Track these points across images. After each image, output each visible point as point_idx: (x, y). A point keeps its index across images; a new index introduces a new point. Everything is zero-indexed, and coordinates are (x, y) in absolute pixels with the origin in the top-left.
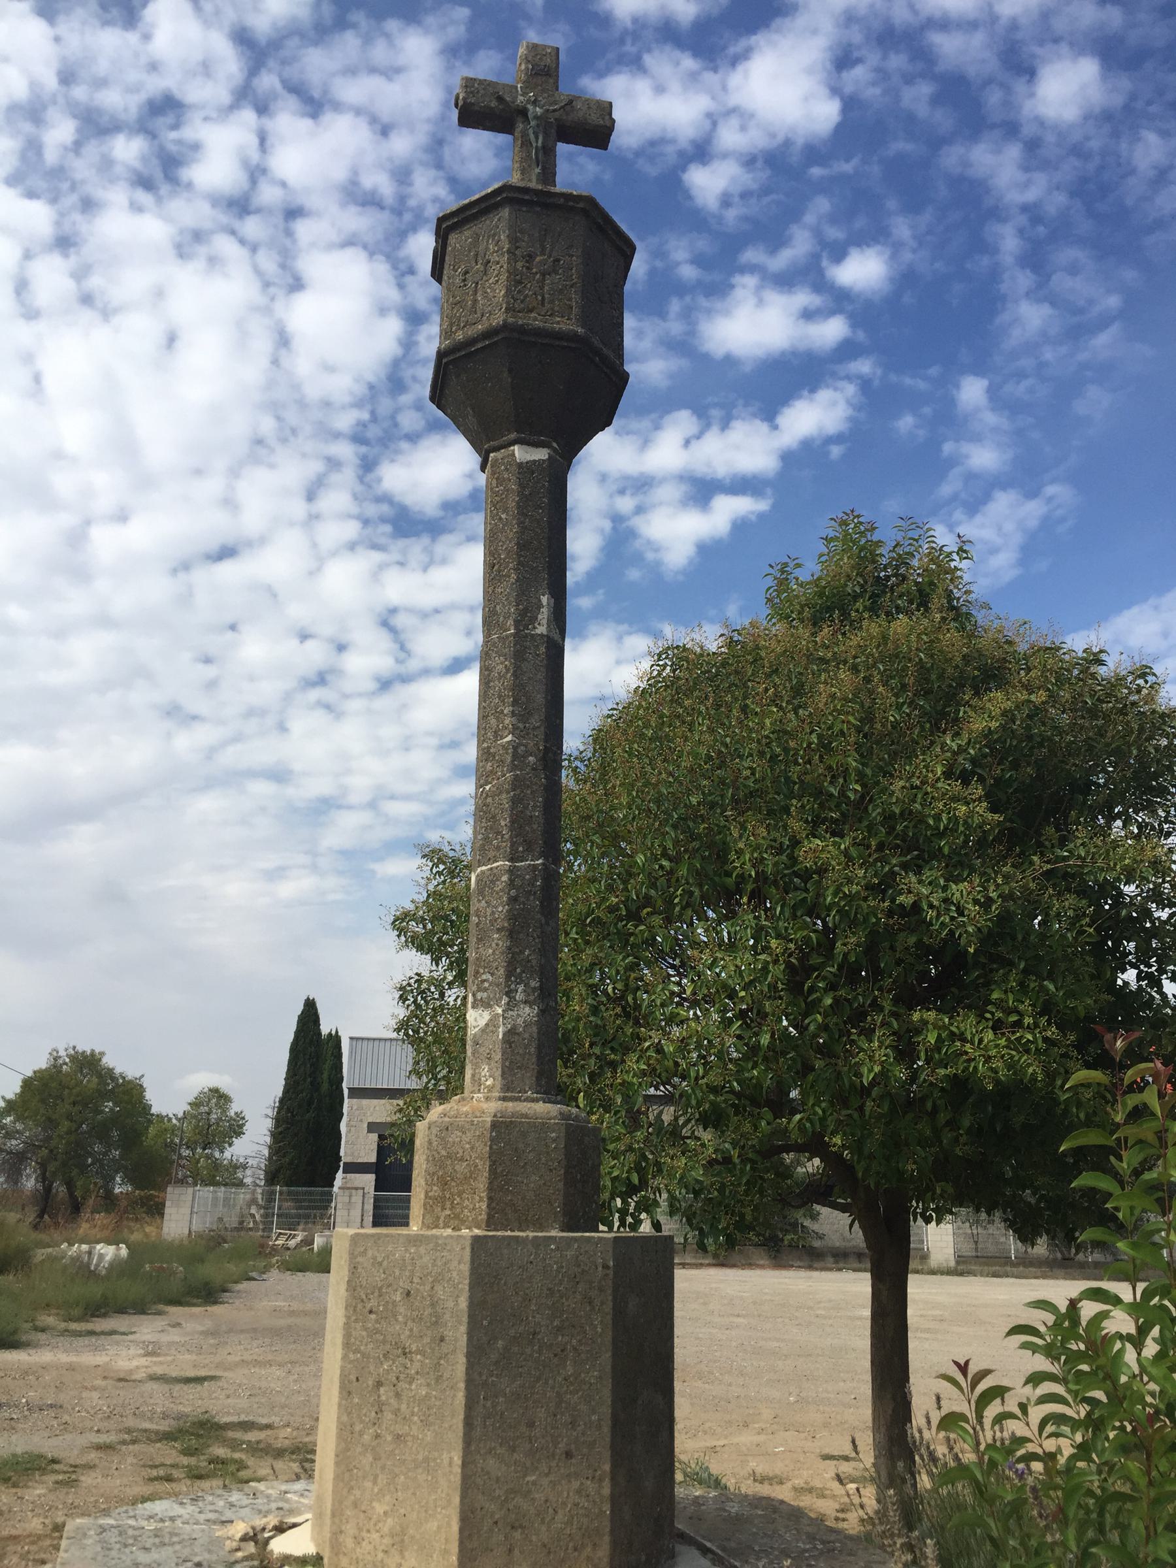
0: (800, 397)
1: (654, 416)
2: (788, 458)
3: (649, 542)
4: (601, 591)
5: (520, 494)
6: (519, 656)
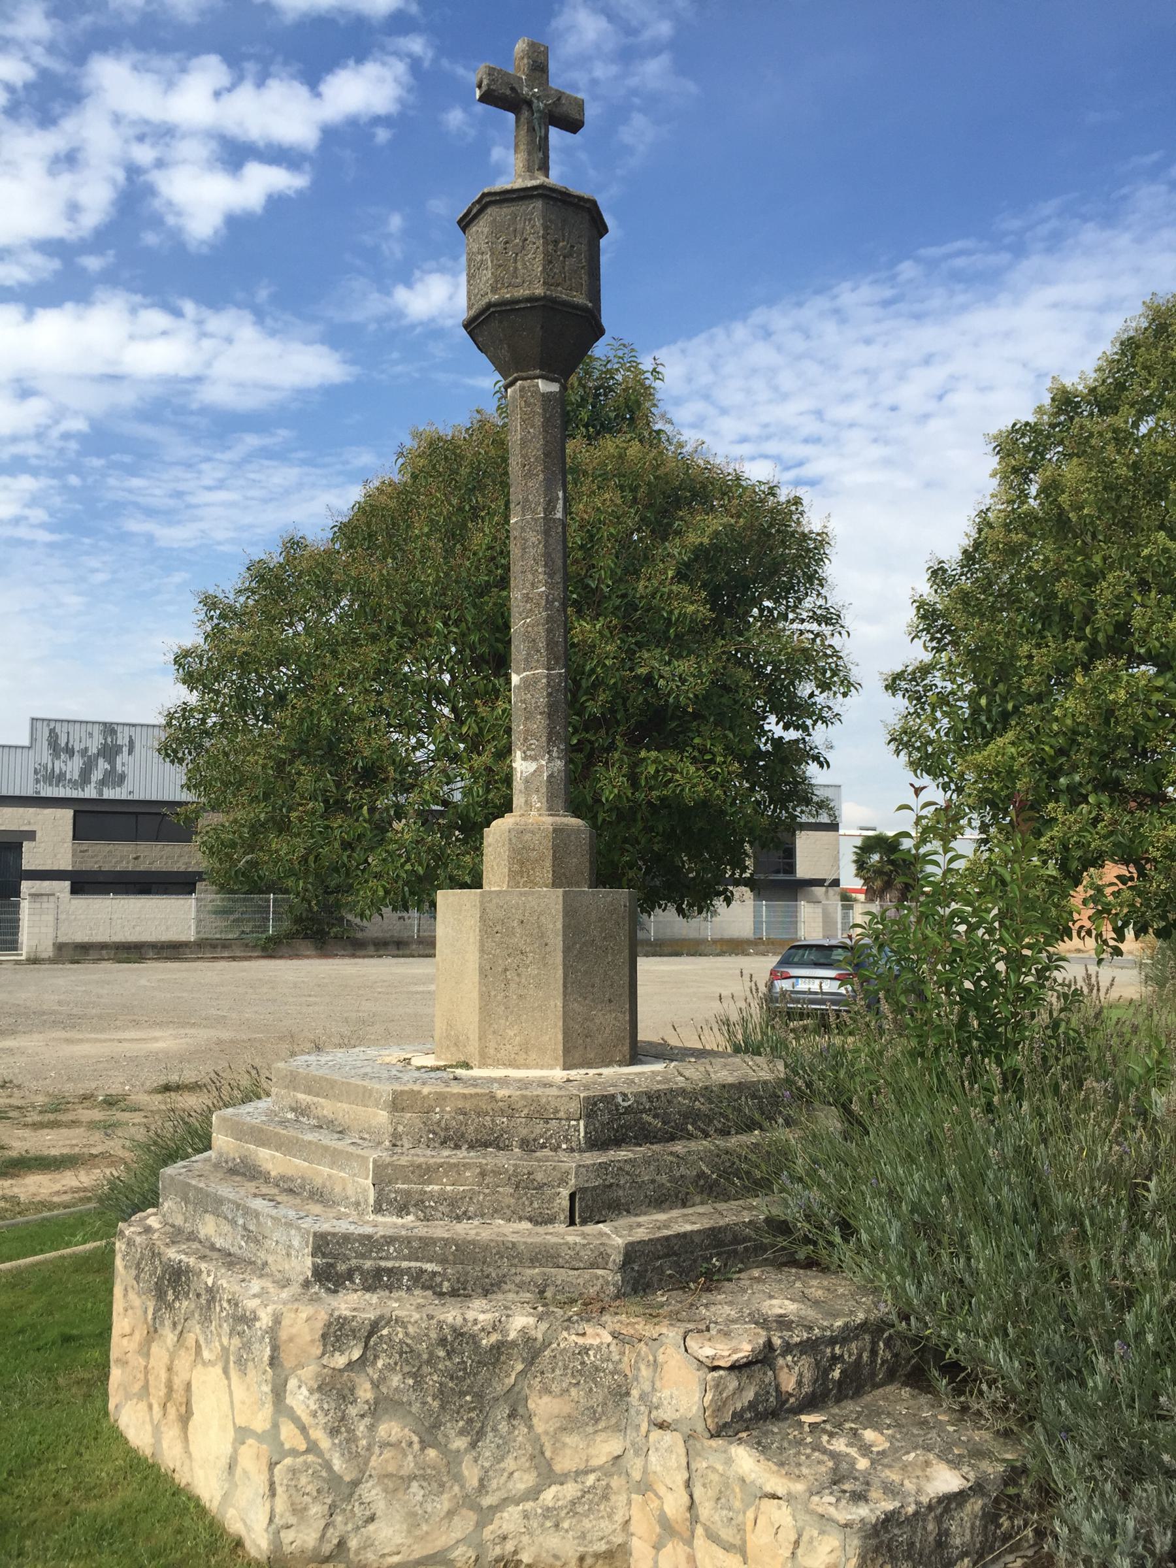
0: (345, 67)
1: (178, 55)
2: (330, 135)
3: (170, 203)
4: (111, 252)
5: (544, 416)
6: (547, 533)
